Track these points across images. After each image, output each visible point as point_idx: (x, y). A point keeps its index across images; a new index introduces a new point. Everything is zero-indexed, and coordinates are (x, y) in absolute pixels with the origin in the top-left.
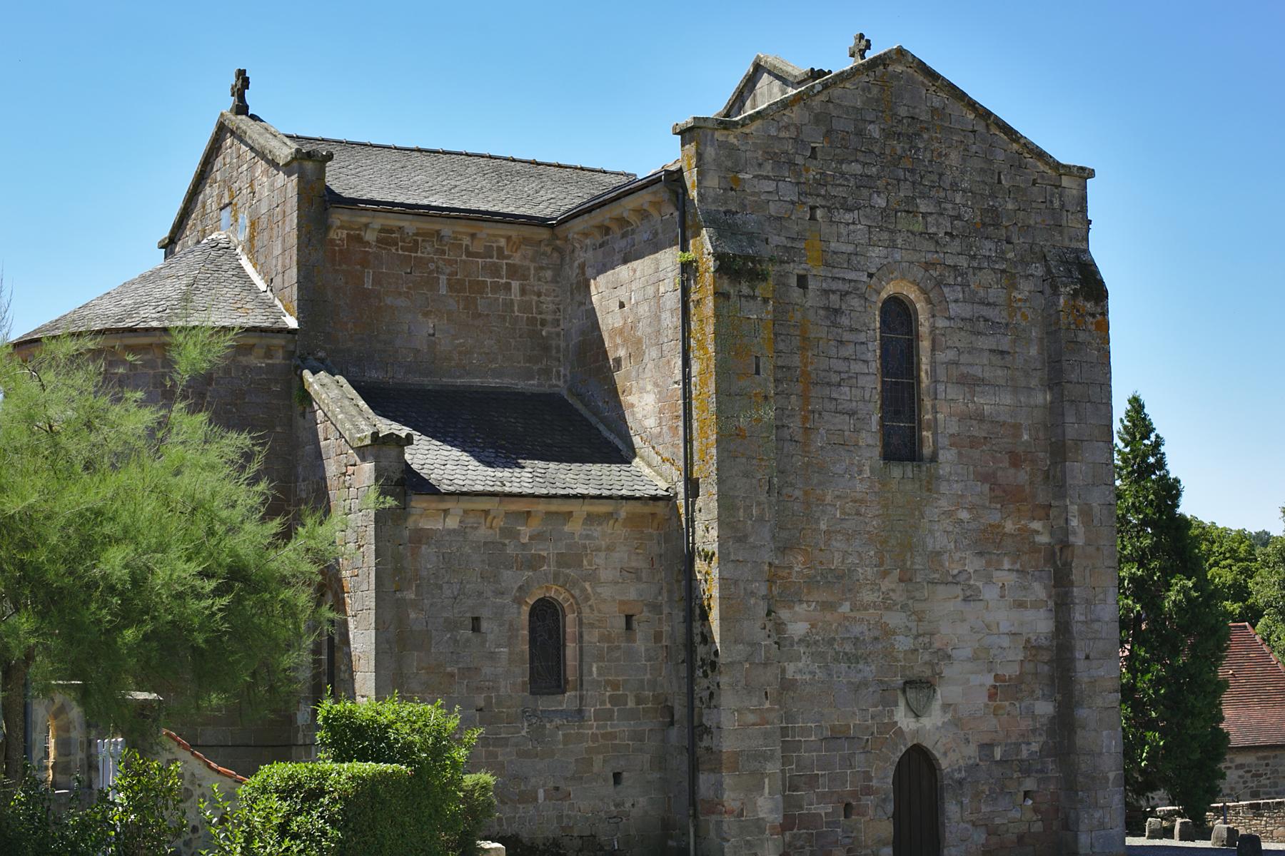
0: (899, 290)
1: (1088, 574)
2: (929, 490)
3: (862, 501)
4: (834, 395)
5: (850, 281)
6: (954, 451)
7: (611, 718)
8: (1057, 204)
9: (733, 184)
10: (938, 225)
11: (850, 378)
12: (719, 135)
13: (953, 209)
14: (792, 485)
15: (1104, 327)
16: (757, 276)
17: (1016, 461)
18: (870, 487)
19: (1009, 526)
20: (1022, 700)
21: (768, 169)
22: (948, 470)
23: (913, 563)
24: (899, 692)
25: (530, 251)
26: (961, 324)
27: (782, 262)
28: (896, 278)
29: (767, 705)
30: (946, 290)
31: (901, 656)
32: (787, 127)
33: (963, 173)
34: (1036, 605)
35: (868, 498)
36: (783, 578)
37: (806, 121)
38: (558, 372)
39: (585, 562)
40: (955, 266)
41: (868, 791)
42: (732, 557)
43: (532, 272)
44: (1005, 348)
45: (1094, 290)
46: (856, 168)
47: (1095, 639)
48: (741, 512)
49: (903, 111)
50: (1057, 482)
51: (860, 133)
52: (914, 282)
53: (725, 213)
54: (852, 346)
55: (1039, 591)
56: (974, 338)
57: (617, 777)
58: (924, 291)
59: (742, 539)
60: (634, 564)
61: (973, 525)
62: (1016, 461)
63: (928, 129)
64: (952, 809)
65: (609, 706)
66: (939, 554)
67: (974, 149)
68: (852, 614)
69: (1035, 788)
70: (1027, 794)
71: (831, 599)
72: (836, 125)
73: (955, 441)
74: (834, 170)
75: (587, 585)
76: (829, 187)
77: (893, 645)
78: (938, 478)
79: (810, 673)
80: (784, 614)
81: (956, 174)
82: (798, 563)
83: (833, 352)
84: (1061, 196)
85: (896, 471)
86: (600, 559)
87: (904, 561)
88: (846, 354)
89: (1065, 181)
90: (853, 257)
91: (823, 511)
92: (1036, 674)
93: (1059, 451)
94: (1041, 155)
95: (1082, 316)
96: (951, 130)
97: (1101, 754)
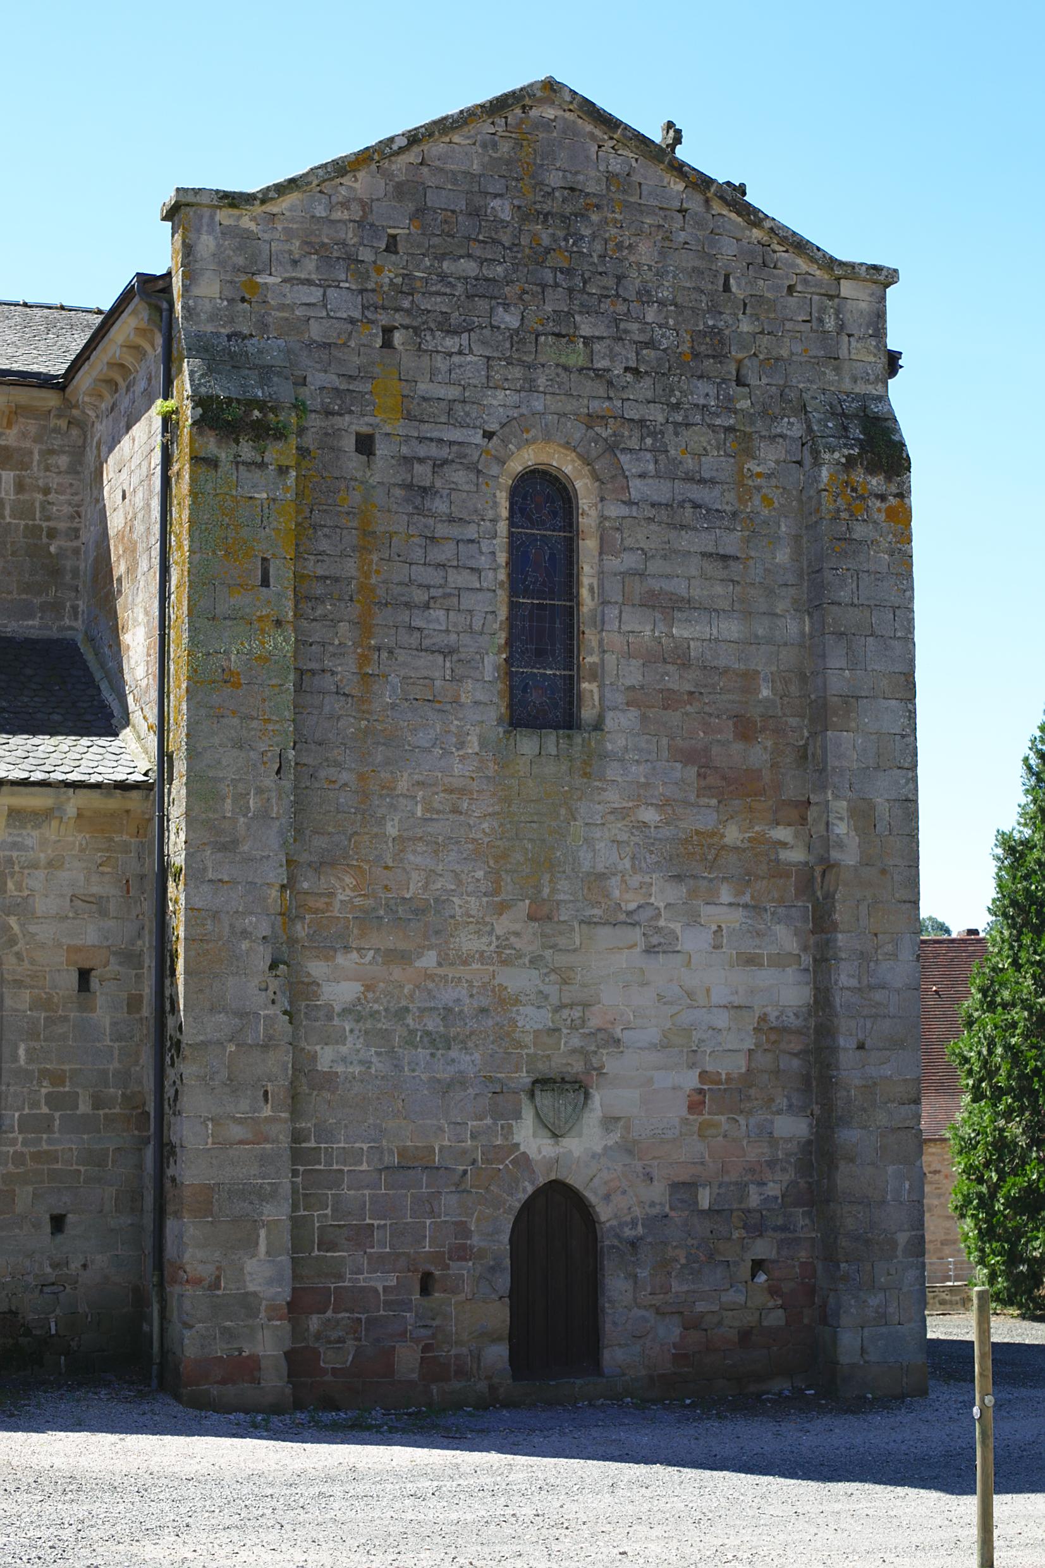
0: (543, 458)
1: (863, 909)
2: (585, 775)
3: (462, 791)
4: (417, 622)
5: (451, 443)
6: (633, 713)
7: (49, 1129)
8: (830, 324)
9: (245, 293)
10: (612, 356)
11: (446, 596)
12: (224, 216)
13: (641, 331)
14: (337, 764)
15: (901, 516)
16: (263, 432)
17: (746, 730)
18: (479, 769)
19: (733, 835)
20: (750, 1113)
21: (310, 267)
22: (621, 742)
23: (553, 891)
24: (523, 1097)
25: (32, 427)
26: (650, 513)
27: (329, 413)
28: (534, 441)
29: (267, 1112)
30: (624, 458)
31: (529, 1039)
32: (345, 205)
33: (660, 274)
34: (779, 961)
35: (475, 785)
36: (316, 911)
37: (381, 194)
38: (75, 608)
39: (10, 885)
40: (641, 421)
41: (462, 1253)
42: (210, 875)
43: (36, 457)
44: (730, 550)
45: (882, 451)
46: (469, 267)
47: (875, 1017)
48: (228, 804)
49: (554, 179)
50: (810, 759)
51: (475, 213)
52: (567, 445)
53: (229, 337)
54: (453, 545)
55: (785, 938)
56: (673, 534)
57: (58, 1223)
58: (587, 461)
59: (228, 847)
60: (95, 890)
61: (666, 832)
62: (746, 730)
63: (598, 206)
64: (617, 1287)
65: (45, 1110)
66: (602, 877)
67: (682, 236)
68: (440, 971)
69: (773, 1255)
70: (758, 1265)
71: (402, 945)
72: (432, 200)
73: (636, 698)
74: (429, 270)
75: (13, 921)
76: (418, 297)
77: (513, 1021)
78: (604, 756)
79: (361, 1062)
80: (316, 968)
81: (649, 276)
82: (344, 890)
83: (417, 554)
84: (838, 312)
85: (527, 744)
86: (36, 881)
87: (538, 888)
88: (441, 558)
89: (847, 288)
90: (458, 406)
91: (391, 805)
92: (777, 1072)
93: (821, 714)
94: (800, 246)
95: (862, 498)
96: (640, 208)
97: (883, 1202)
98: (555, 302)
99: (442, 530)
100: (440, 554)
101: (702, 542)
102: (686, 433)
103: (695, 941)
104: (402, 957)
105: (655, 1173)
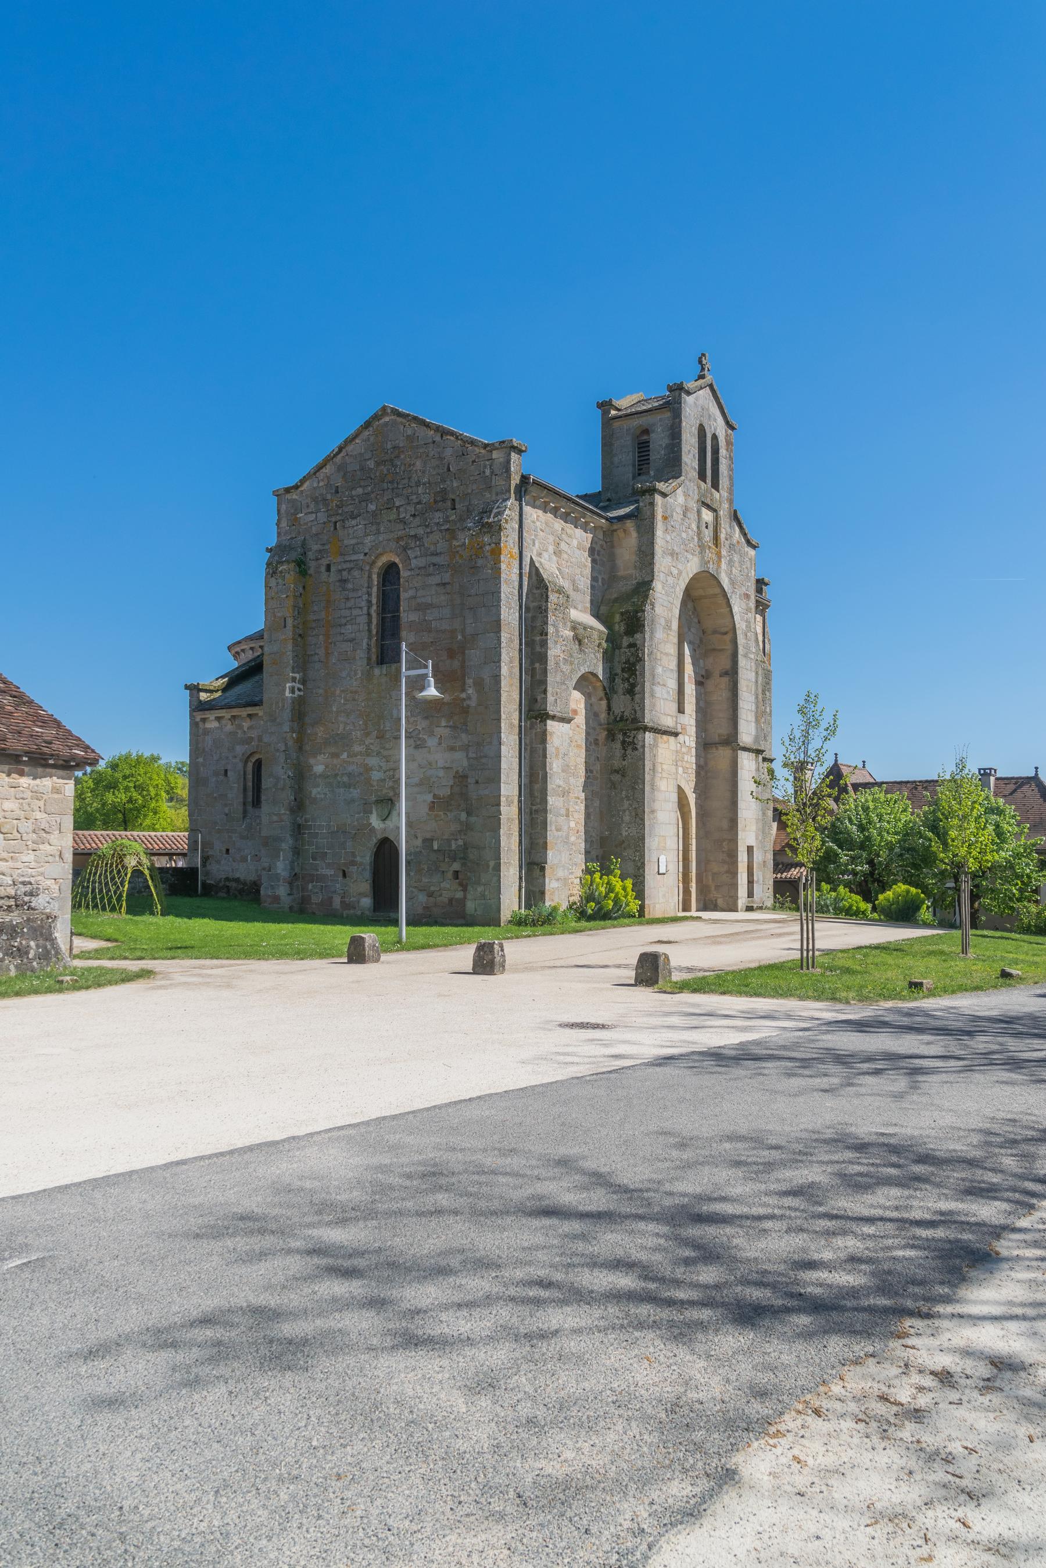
3: (356, 692)
8: (488, 472)
27: (317, 559)
41: (353, 863)
44: (447, 581)
46: (360, 491)
82: (320, 732)
98: (387, 496)
99: (351, 595)
100: (349, 604)
101: (436, 579)
102: (431, 536)
103: (432, 742)
104: (336, 755)
105: (419, 835)
